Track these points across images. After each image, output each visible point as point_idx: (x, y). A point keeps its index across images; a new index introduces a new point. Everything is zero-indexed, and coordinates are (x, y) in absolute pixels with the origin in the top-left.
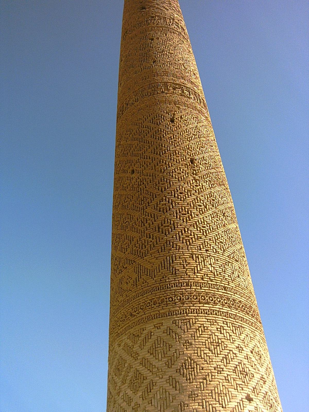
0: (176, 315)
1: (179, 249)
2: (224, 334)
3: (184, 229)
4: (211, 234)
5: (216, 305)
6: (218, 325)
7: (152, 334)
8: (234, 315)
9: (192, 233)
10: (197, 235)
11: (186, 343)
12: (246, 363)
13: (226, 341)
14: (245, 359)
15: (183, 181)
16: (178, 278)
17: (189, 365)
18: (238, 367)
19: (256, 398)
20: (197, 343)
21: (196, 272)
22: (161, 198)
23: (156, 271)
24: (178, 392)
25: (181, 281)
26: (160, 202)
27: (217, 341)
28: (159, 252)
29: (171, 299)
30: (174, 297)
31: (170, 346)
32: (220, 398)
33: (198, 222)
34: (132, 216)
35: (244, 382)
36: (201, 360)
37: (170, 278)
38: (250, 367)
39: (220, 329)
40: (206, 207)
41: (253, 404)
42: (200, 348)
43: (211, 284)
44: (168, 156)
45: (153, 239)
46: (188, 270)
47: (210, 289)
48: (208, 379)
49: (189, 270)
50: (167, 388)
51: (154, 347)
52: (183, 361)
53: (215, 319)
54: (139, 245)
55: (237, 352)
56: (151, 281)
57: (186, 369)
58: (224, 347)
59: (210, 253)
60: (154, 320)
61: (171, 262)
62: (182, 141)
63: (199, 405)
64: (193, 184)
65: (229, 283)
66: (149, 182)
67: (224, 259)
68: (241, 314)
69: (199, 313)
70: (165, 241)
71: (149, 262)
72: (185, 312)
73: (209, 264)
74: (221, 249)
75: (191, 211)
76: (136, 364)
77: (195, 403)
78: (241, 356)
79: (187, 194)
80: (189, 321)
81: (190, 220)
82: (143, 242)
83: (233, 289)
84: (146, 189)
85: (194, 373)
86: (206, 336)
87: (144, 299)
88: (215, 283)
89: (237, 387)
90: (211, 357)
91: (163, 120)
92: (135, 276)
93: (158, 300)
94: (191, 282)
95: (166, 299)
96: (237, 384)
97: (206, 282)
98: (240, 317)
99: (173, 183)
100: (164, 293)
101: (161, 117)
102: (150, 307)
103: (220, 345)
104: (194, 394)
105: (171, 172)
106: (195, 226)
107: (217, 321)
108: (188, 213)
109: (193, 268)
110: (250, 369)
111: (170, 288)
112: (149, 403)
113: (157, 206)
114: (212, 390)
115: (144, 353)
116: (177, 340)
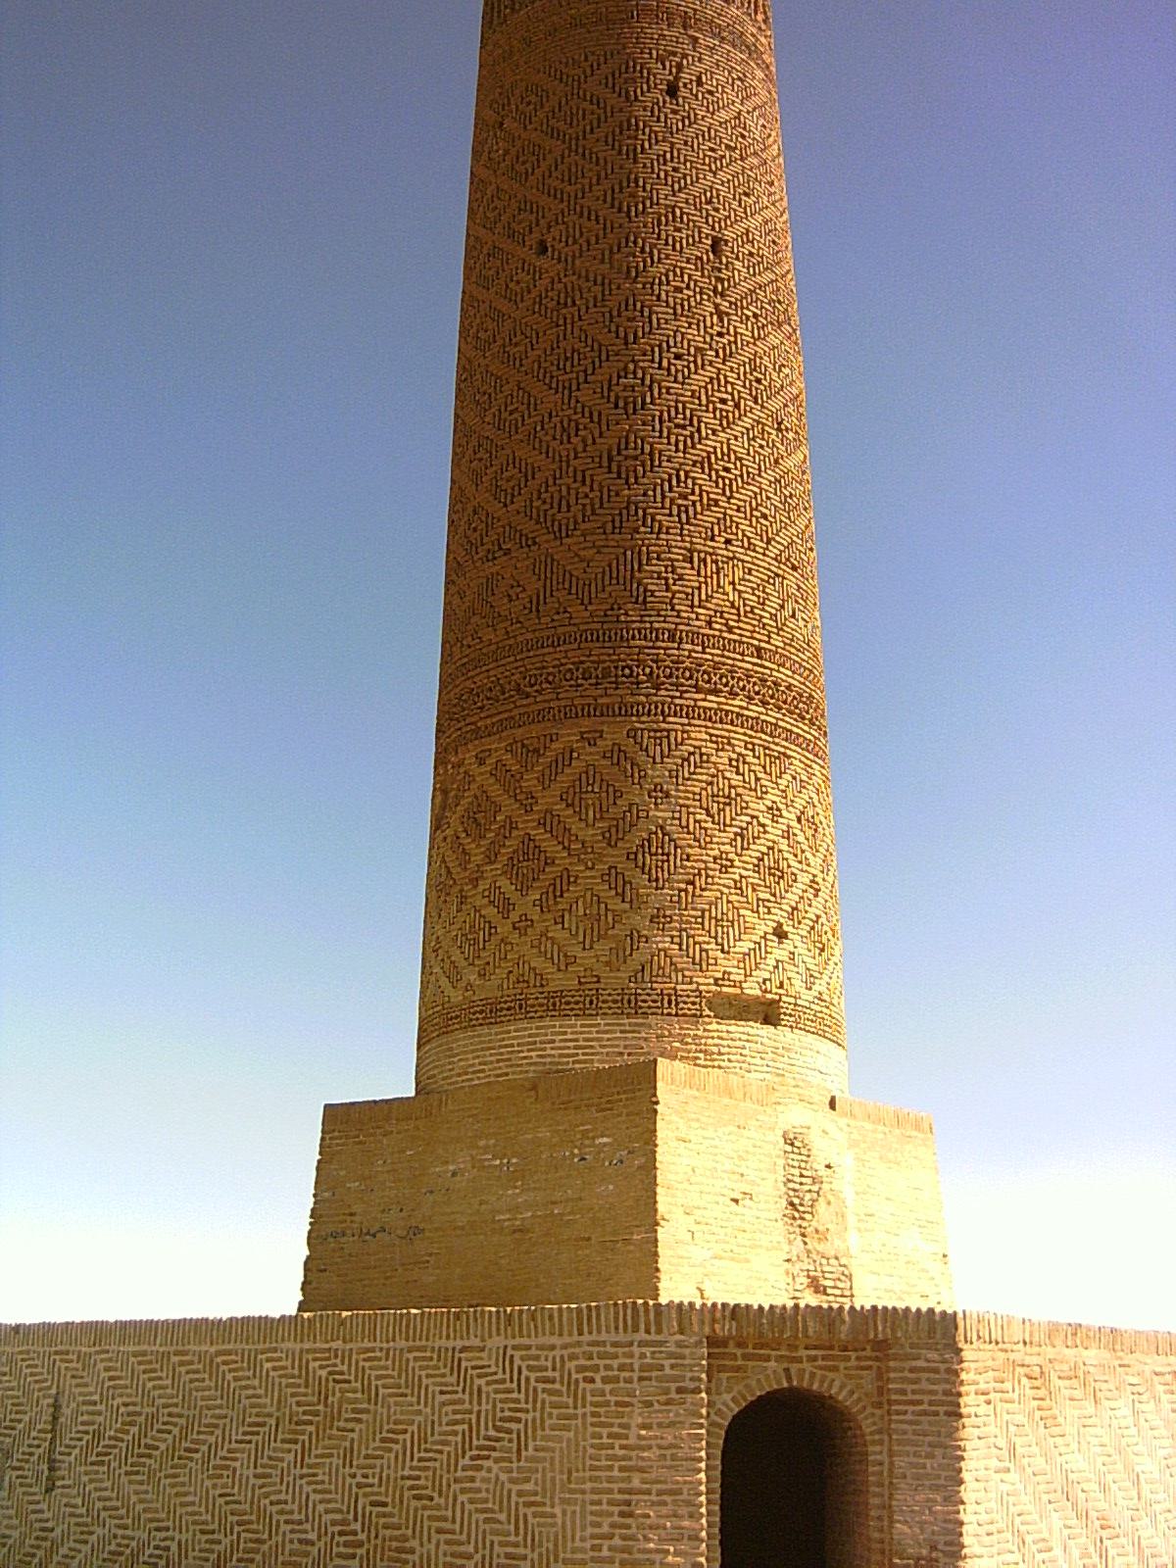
0: (637, 715)
1: (659, 533)
2: (743, 775)
3: (678, 471)
4: (744, 491)
5: (734, 699)
6: (734, 751)
7: (575, 755)
8: (771, 724)
9: (697, 488)
10: (708, 493)
11: (655, 791)
12: (784, 847)
13: (747, 792)
14: (783, 837)
15: (687, 317)
16: (650, 616)
17: (658, 848)
18: (766, 857)
19: (795, 931)
20: (682, 795)
21: (696, 603)
22: (622, 365)
23: (593, 585)
24: (627, 906)
25: (656, 625)
26: (619, 377)
27: (727, 793)
28: (605, 533)
29: (627, 671)
30: (638, 667)
31: (618, 794)
32: (719, 929)
33: (715, 453)
34: (532, 399)
35: (774, 895)
36: (688, 836)
37: (631, 613)
38: (791, 857)
39: (737, 761)
40: (737, 406)
41: (788, 945)
42: (688, 807)
43: (730, 640)
44: (653, 223)
45: (592, 490)
46: (677, 595)
47: (726, 653)
48: (698, 885)
49: (680, 595)
50: (602, 894)
51: (578, 790)
52: (645, 835)
53: (727, 734)
54: (552, 497)
55: (768, 822)
56: (579, 612)
57: (651, 855)
58: (742, 808)
59: (734, 549)
60: (580, 721)
61: (636, 567)
62: (694, 171)
63: (672, 943)
64: (712, 328)
65: (769, 637)
66: (591, 305)
67: (764, 568)
68: (788, 722)
69: (693, 718)
70: (625, 504)
71: (576, 555)
72: (659, 710)
73: (730, 583)
74: (761, 536)
75: (699, 417)
76: (528, 821)
77: (663, 936)
78: (774, 832)
79: (695, 362)
80: (668, 737)
81: (693, 447)
82: (564, 493)
83: (777, 653)
84: (580, 323)
85: (669, 866)
86: (704, 777)
87: (557, 656)
88: (738, 638)
89: (758, 906)
90: (709, 832)
91: (645, 87)
92: (534, 585)
93: (596, 669)
94: (681, 631)
95: (616, 668)
96: (758, 899)
97: (717, 633)
98: (784, 728)
99: (658, 319)
100: (611, 651)
101: (641, 72)
102: (573, 682)
103: (733, 802)
104: (665, 917)
105: (657, 281)
106: (706, 465)
107: (733, 741)
108: (691, 425)
109: (690, 591)
110: (792, 863)
111: (627, 640)
112: (556, 923)
113: (609, 390)
114: (703, 911)
115: (548, 799)
116: (636, 781)
